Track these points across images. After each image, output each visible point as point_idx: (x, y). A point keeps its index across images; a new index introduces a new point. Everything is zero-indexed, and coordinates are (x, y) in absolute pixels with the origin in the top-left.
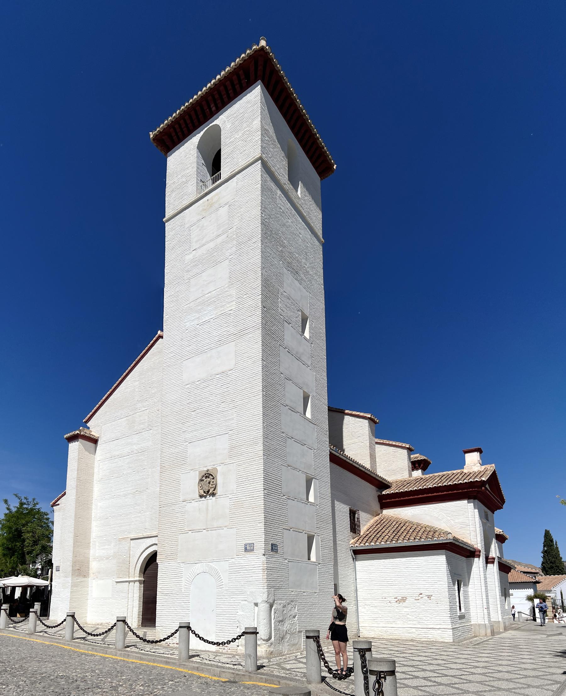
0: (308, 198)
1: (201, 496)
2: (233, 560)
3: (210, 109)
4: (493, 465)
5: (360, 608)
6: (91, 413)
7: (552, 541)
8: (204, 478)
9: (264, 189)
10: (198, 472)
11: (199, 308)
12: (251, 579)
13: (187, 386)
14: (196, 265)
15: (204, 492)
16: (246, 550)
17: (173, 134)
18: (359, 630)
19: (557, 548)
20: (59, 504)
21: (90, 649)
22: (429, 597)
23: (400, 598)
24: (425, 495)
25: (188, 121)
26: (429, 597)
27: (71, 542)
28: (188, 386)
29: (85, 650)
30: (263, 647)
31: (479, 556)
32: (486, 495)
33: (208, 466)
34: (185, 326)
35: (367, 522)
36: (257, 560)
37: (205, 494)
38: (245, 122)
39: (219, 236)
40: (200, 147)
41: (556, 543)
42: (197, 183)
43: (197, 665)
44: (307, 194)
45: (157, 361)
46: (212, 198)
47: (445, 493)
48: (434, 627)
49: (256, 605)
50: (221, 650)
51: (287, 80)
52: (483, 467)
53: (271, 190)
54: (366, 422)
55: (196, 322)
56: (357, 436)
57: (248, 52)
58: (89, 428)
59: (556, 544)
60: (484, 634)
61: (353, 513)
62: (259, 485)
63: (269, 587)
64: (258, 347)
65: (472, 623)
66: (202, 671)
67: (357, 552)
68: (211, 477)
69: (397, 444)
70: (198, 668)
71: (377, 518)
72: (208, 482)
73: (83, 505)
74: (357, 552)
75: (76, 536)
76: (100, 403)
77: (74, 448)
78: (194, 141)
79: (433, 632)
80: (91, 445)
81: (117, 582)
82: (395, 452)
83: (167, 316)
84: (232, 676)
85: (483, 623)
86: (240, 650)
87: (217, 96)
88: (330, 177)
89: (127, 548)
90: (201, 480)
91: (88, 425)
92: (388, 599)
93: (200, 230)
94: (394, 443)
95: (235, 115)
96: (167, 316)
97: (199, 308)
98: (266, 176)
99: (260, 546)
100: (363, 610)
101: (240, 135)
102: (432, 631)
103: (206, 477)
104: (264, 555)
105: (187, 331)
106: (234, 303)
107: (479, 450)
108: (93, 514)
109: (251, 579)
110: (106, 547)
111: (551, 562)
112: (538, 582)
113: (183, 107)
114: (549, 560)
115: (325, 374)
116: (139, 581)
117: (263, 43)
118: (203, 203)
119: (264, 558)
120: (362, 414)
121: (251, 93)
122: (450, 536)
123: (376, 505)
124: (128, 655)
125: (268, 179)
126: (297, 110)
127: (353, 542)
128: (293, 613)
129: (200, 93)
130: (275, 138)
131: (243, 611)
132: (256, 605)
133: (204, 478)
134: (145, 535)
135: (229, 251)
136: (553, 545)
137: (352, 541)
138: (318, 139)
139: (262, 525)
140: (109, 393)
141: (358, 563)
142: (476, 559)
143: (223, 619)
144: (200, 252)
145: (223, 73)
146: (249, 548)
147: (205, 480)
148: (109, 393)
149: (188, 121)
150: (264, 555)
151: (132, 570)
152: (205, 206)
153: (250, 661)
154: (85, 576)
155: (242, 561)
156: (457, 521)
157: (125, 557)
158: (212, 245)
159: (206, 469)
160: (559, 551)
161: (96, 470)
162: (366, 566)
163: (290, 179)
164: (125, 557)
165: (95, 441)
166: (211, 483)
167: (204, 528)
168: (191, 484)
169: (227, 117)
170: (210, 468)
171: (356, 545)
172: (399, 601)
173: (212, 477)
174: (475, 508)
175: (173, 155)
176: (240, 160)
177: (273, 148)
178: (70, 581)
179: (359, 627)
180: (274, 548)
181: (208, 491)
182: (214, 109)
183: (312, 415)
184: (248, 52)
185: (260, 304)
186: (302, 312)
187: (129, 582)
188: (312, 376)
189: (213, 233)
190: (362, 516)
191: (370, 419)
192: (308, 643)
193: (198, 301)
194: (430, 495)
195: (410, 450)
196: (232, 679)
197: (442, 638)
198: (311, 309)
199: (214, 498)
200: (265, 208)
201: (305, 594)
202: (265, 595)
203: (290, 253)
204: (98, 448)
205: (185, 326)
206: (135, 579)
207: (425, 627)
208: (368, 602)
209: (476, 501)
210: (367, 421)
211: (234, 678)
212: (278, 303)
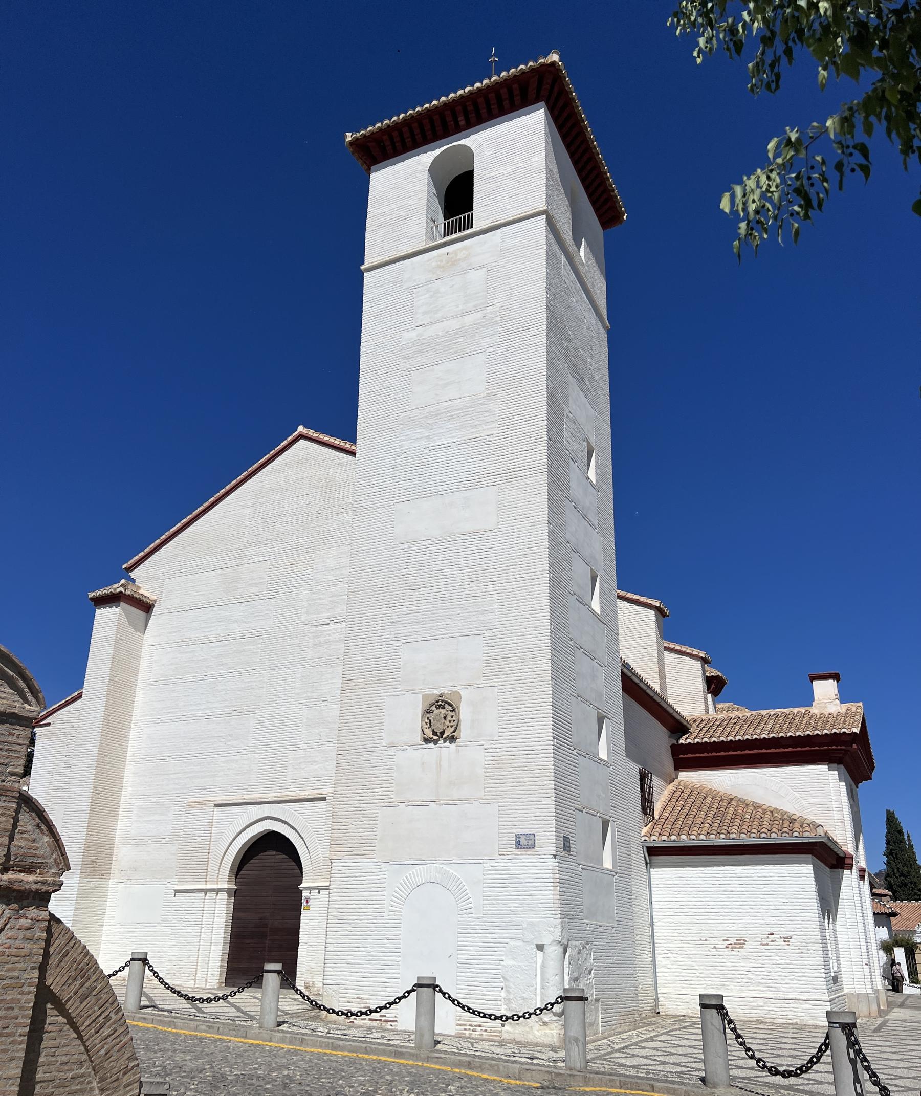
0: (592, 261)
1: (427, 741)
2: (493, 863)
3: (457, 122)
4: (861, 704)
5: (659, 958)
6: (142, 554)
7: (900, 832)
8: (433, 708)
9: (550, 255)
10: (420, 696)
11: (430, 421)
12: (529, 900)
13: (402, 547)
14: (422, 351)
15: (435, 733)
16: (519, 845)
17: (388, 143)
18: (657, 1000)
19: (911, 847)
20: (49, 724)
21: (204, 1027)
22: (787, 939)
23: (733, 940)
24: (755, 751)
25: (417, 131)
26: (787, 939)
27: (86, 806)
28: (406, 546)
29: (190, 1029)
30: (552, 1026)
31: (850, 867)
32: (849, 754)
33: (444, 688)
34: (401, 446)
35: (662, 794)
36: (542, 865)
37: (435, 738)
38: (515, 155)
39: (468, 312)
40: (434, 170)
41: (909, 837)
42: (427, 222)
43: (467, 1059)
44: (591, 257)
45: (293, 478)
46: (455, 252)
47: (790, 749)
48: (798, 997)
49: (540, 947)
50: (467, 1032)
51: (578, 104)
52: (845, 707)
53: (555, 257)
54: (651, 614)
55: (423, 443)
56: (637, 634)
57: (531, 64)
58: (134, 581)
59: (909, 840)
60: (867, 1013)
61: (643, 777)
62: (545, 729)
63: (564, 915)
64: (542, 500)
65: (846, 991)
66: (481, 1068)
67: (654, 852)
68: (448, 707)
69: (683, 649)
70: (469, 1063)
71: (671, 787)
72: (442, 716)
73: (115, 729)
74: (654, 852)
75: (96, 792)
76: (163, 537)
77: (107, 620)
78: (425, 159)
79: (795, 1006)
80: (139, 614)
81: (177, 891)
82: (679, 663)
83: (365, 425)
84: (547, 1077)
85: (864, 991)
86: (508, 1032)
87: (470, 108)
88: (615, 229)
89: (204, 823)
90: (429, 712)
91: (132, 575)
92: (713, 941)
93: (431, 297)
94: (678, 648)
95: (500, 140)
96: (365, 425)
97: (430, 421)
98: (551, 236)
99: (548, 841)
100: (664, 962)
101: (509, 170)
102: (793, 1004)
103: (438, 707)
104: (555, 856)
105: (405, 456)
106: (496, 425)
107: (835, 677)
108: (130, 749)
109: (529, 900)
110: (156, 817)
111: (902, 875)
112: (894, 915)
113: (411, 112)
114: (898, 869)
115: (613, 539)
116: (228, 891)
117: (555, 57)
118: (439, 256)
119: (554, 863)
120: (643, 599)
121: (528, 116)
122: (820, 831)
123: (668, 762)
124: (302, 1041)
125: (553, 241)
126: (585, 141)
127: (643, 833)
128: (588, 965)
129: (443, 99)
130: (559, 179)
131: (514, 959)
132: (540, 947)
133: (433, 708)
134: (248, 798)
135: (487, 340)
136: (902, 841)
137: (645, 830)
138: (608, 179)
139: (551, 803)
140: (185, 521)
141: (653, 871)
142: (846, 872)
143: (472, 972)
144: (430, 332)
145: (486, 82)
146: (524, 843)
147: (437, 712)
148: (185, 521)
149: (417, 131)
150: (555, 856)
151: (212, 867)
152: (441, 261)
153: (577, 1049)
154: (102, 877)
155: (510, 866)
156: (811, 801)
157: (199, 839)
158: (454, 324)
159: (437, 692)
160: (914, 854)
161: (144, 663)
162: (669, 880)
163: (574, 239)
164: (199, 839)
165: (147, 607)
166: (449, 718)
167: (433, 799)
168: (408, 718)
169: (486, 140)
170: (446, 692)
171: (653, 838)
172: (731, 946)
173: (450, 708)
174: (840, 780)
175: (382, 171)
176: (508, 207)
177: (557, 195)
178: (76, 886)
179: (657, 994)
180: (566, 844)
181: (442, 733)
182: (462, 123)
183: (601, 607)
184: (531, 64)
185: (545, 435)
186: (588, 443)
187: (206, 891)
188: (600, 546)
189: (457, 306)
190: (656, 782)
191: (658, 610)
192: (708, 1017)
193: (427, 410)
194: (764, 751)
195: (704, 661)
196: (546, 1084)
197: (813, 1018)
198: (596, 437)
199: (453, 745)
200: (550, 284)
201: (601, 929)
202: (558, 931)
203: (575, 349)
204: (151, 621)
205: (401, 446)
206: (220, 886)
207: (782, 996)
208: (673, 947)
209: (842, 766)
210: (652, 612)
211: (551, 1081)
212: (562, 430)
